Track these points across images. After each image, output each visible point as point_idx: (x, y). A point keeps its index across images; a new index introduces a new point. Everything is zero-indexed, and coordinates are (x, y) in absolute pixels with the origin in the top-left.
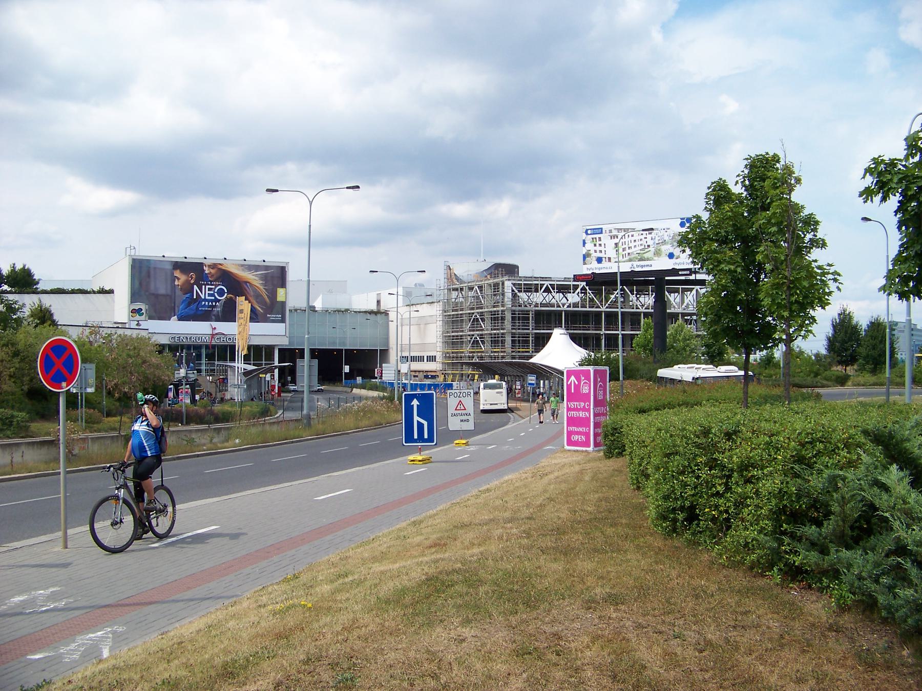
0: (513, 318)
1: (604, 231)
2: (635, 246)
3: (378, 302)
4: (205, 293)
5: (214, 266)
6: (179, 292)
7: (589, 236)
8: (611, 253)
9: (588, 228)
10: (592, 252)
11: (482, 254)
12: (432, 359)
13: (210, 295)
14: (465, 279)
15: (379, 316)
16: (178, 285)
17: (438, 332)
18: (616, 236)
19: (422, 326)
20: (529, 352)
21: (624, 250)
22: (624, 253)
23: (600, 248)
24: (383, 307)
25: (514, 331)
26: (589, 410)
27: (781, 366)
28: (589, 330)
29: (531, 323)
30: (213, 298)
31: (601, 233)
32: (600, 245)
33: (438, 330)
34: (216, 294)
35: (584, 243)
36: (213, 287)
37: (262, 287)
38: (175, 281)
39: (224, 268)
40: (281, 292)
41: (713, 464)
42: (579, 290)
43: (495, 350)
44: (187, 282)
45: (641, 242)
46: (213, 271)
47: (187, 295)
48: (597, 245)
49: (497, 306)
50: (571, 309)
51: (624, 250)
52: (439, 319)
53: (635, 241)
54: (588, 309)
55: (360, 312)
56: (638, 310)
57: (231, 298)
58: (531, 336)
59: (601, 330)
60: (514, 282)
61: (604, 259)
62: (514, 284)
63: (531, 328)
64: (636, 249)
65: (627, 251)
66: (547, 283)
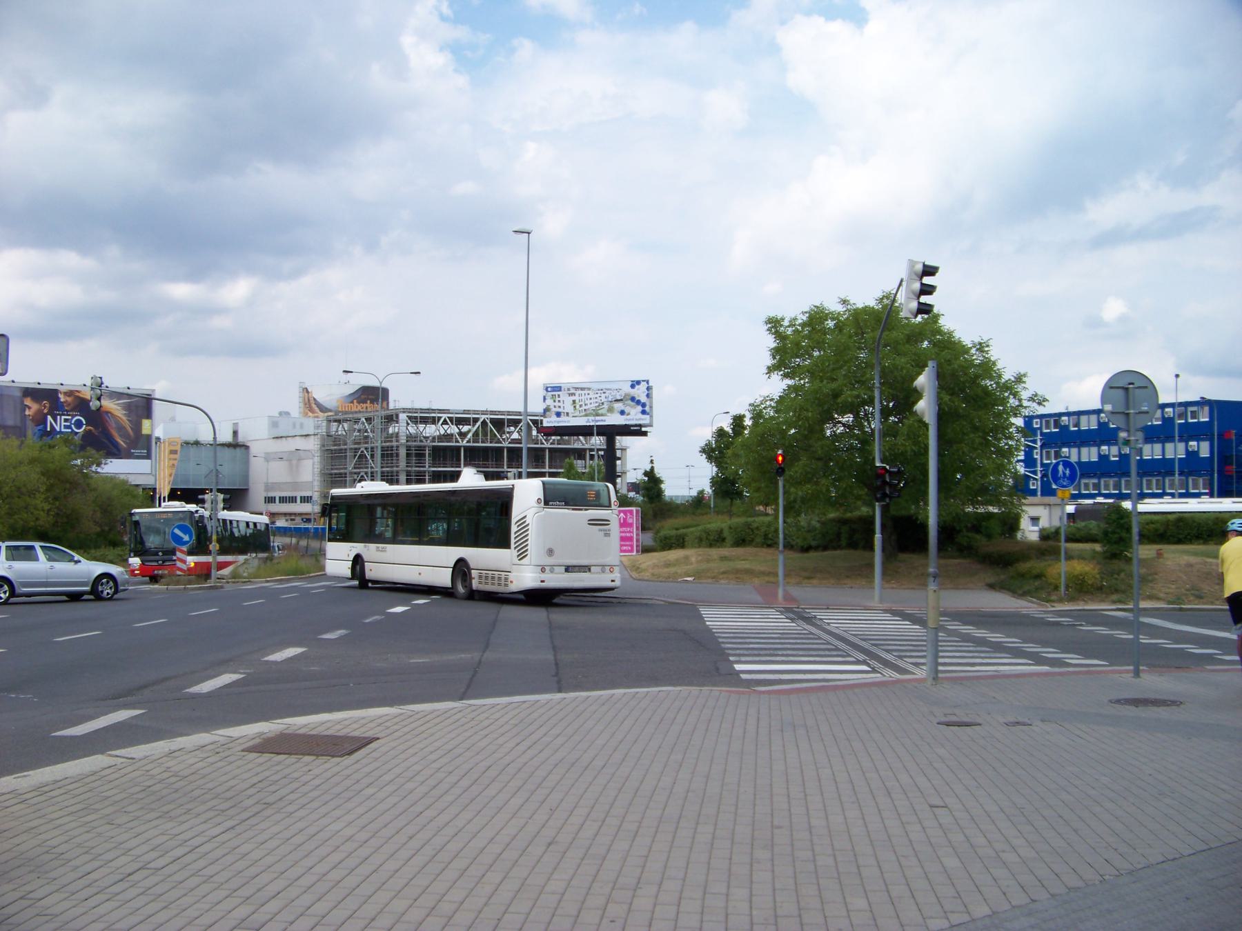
0: (408, 455)
1: (562, 389)
2: (591, 404)
3: (235, 433)
4: (59, 424)
5: (70, 393)
6: (30, 424)
7: (549, 393)
8: (569, 408)
9: (548, 386)
10: (552, 407)
11: (878, 537)
12: (306, 500)
13: (66, 427)
14: (327, 405)
15: (238, 450)
16: (29, 415)
17: (316, 470)
18: (573, 394)
19: (294, 462)
21: (581, 406)
22: (580, 409)
23: (559, 404)
24: (241, 439)
25: (409, 469)
26: (633, 532)
27: (712, 506)
28: (487, 467)
29: (427, 460)
30: (70, 430)
31: (560, 390)
32: (559, 401)
33: (316, 466)
34: (73, 426)
35: (545, 399)
36: (70, 417)
37: (124, 418)
38: (25, 411)
39: (82, 396)
40: (146, 424)
41: (749, 528)
42: (479, 423)
44: (39, 412)
45: (596, 400)
46: (69, 399)
47: (41, 426)
48: (557, 401)
49: (391, 441)
50: (471, 444)
51: (581, 406)
52: (316, 455)
53: (591, 399)
54: (489, 445)
56: (542, 446)
57: (90, 430)
58: (427, 474)
59: (503, 468)
60: (410, 415)
61: (562, 414)
62: (410, 418)
63: (427, 465)
64: (591, 406)
65: (584, 407)
66: (444, 416)
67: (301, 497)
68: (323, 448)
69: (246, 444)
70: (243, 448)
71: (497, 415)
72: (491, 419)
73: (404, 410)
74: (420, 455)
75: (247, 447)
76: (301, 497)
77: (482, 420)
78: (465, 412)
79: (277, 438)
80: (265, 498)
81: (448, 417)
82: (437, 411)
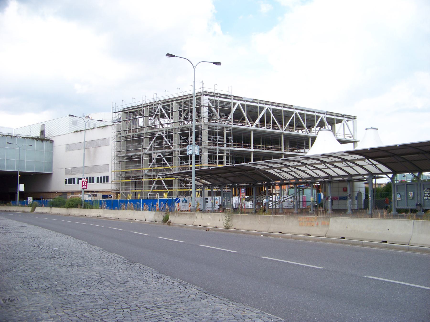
3: (42, 132)
12: (105, 179)
15: (45, 142)
24: (47, 136)
55: (27, 138)
62: (212, 101)
67: (98, 178)
68: (119, 136)
69: (51, 139)
70: (49, 142)
71: (277, 106)
72: (273, 109)
73: (206, 94)
74: (138, 140)
75: (52, 142)
76: (98, 178)
77: (266, 109)
78: (255, 101)
79: (77, 132)
80: (66, 179)
81: (241, 104)
82: (233, 98)
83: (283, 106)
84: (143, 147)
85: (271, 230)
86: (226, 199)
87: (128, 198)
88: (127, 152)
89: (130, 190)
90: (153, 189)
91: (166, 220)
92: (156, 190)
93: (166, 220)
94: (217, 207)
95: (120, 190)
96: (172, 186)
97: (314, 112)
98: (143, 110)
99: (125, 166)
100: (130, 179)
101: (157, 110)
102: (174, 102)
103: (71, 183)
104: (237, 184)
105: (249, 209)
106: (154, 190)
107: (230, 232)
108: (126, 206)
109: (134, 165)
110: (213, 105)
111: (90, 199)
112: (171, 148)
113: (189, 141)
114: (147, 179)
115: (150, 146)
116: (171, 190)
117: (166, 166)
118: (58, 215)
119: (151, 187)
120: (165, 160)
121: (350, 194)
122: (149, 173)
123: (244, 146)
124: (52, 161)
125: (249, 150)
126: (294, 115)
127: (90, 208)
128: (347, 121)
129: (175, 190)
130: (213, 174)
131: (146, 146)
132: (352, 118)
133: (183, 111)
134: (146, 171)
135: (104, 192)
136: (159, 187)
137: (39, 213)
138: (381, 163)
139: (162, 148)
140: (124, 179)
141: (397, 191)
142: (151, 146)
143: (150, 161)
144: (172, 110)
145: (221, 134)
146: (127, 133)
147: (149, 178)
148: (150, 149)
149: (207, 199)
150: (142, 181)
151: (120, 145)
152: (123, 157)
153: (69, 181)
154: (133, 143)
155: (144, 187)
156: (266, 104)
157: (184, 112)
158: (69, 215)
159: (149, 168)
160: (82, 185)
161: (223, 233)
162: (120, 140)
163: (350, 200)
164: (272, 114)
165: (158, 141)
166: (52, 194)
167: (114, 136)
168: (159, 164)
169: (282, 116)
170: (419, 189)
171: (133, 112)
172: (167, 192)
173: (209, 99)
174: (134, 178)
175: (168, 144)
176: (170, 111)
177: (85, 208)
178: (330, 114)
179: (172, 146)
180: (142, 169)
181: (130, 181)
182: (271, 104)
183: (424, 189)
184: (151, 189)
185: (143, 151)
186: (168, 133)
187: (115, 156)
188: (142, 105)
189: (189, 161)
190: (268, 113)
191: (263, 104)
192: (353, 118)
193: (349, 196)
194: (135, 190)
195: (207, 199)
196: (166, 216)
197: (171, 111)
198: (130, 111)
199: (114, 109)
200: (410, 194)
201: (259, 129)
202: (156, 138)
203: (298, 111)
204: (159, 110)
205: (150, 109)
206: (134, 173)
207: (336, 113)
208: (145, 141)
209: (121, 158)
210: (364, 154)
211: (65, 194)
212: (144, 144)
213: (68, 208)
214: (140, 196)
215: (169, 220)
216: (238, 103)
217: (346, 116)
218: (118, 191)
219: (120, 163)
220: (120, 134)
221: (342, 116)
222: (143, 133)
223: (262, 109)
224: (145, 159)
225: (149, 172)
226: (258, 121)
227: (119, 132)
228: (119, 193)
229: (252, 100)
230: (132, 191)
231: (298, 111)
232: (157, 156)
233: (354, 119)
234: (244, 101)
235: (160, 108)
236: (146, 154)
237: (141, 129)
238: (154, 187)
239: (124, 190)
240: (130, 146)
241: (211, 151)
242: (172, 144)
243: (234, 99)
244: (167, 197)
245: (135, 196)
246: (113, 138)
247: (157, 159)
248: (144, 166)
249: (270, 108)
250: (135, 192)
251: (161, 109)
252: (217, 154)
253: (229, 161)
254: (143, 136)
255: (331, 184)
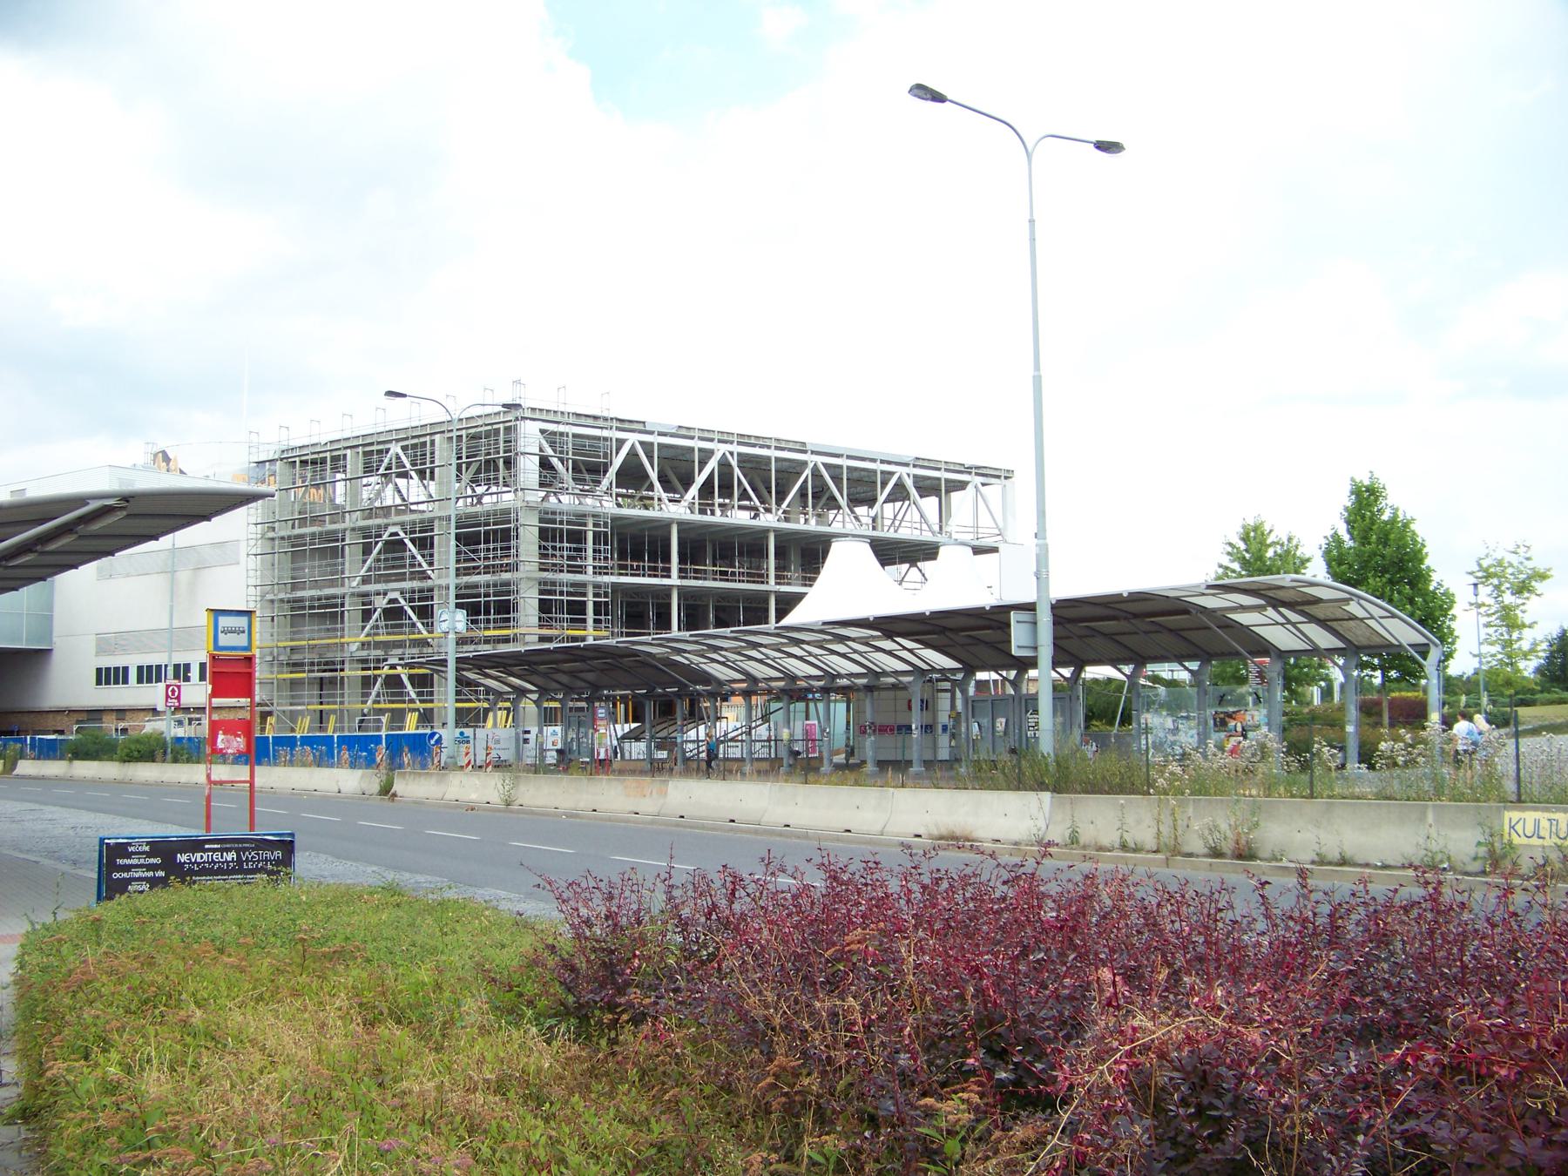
20: (583, 639)
43: (487, 633)
62: (551, 437)
67: (140, 669)
68: (271, 535)
71: (754, 445)
72: (915, 476)
73: (537, 414)
74: (330, 549)
76: (140, 669)
78: (684, 432)
80: (99, 671)
81: (642, 443)
82: (615, 424)
83: (774, 444)
84: (343, 573)
85: (582, 805)
86: (578, 734)
87: (298, 729)
88: (294, 587)
89: (303, 704)
90: (375, 702)
91: (386, 790)
92: (382, 706)
93: (386, 790)
94: (551, 757)
95: (272, 704)
96: (432, 693)
97: (874, 460)
98: (345, 456)
99: (289, 629)
100: (304, 672)
101: (386, 461)
102: (437, 437)
103: (117, 682)
104: (605, 692)
105: (638, 763)
106: (376, 706)
107: (512, 812)
108: (292, 755)
109: (316, 628)
110: (555, 451)
111: (180, 732)
112: (430, 578)
113: (480, 559)
114: (357, 669)
115: (365, 569)
116: (429, 705)
117: (414, 633)
118: (94, 781)
119: (367, 695)
120: (410, 612)
121: (872, 723)
122: (364, 653)
123: (654, 572)
124: (51, 609)
125: (666, 581)
126: (808, 472)
127: (188, 761)
128: (983, 485)
129: (441, 705)
130: (535, 663)
131: (354, 572)
132: (998, 477)
133: (464, 465)
134: (354, 647)
135: (223, 712)
136: (393, 694)
137: (30, 777)
138: (928, 645)
139: (401, 577)
140: (285, 669)
141: (973, 717)
142: (369, 569)
143: (367, 615)
144: (432, 462)
145: (577, 537)
146: (293, 527)
147: (363, 669)
148: (366, 580)
149: (528, 732)
150: (342, 678)
151: (273, 565)
152: (282, 601)
153: (107, 676)
154: (312, 558)
155: (346, 695)
156: (720, 441)
157: (467, 469)
158: (130, 782)
159: (362, 638)
160: (167, 696)
161: (498, 814)
162: (273, 548)
163: (873, 738)
164: (737, 471)
165: (390, 556)
166: (51, 716)
167: (254, 536)
168: (393, 626)
169: (770, 470)
170: (1017, 711)
171: (314, 462)
172: (418, 710)
173: (542, 432)
174: (316, 668)
175: (420, 565)
176: (425, 464)
177: (175, 761)
178: (926, 464)
179: (433, 570)
180: (342, 640)
181: (304, 675)
182: (736, 439)
183: (1027, 711)
184: (370, 702)
185: (343, 585)
186: (420, 532)
187: (259, 599)
188: (339, 440)
189: (482, 617)
190: (724, 465)
191: (712, 440)
192: (1003, 474)
193: (870, 728)
194: (321, 703)
195: (528, 732)
196: (388, 780)
197: (428, 465)
198: (304, 458)
199: (254, 450)
200: (998, 725)
201: (697, 517)
202: (384, 544)
203: (820, 459)
204: (394, 461)
205: (365, 454)
206: (316, 650)
207: (946, 462)
208: (352, 554)
209: (276, 605)
210: (883, 627)
211: (96, 716)
212: (347, 565)
213: (125, 761)
214: (336, 723)
215: (392, 791)
216: (632, 439)
217: (980, 471)
218: (267, 709)
219: (273, 620)
220: (274, 529)
221: (968, 470)
222: (345, 530)
223: (706, 455)
224: (352, 608)
225: (363, 649)
226: (694, 491)
227: (270, 525)
228: (270, 713)
229: (674, 431)
230: (309, 707)
231: (820, 459)
232: (386, 601)
233: (1006, 478)
234: (651, 433)
235: (397, 454)
236: (353, 595)
237: (339, 514)
238: (378, 695)
239: (286, 705)
240: (303, 569)
241: (546, 588)
242: (431, 564)
243: (618, 429)
244: (417, 728)
245: (321, 723)
246: (252, 543)
247: (385, 610)
248: (346, 632)
249: (732, 454)
250: (321, 711)
251: (398, 457)
252: (565, 598)
253: (603, 617)
254: (343, 540)
255: (876, 693)
